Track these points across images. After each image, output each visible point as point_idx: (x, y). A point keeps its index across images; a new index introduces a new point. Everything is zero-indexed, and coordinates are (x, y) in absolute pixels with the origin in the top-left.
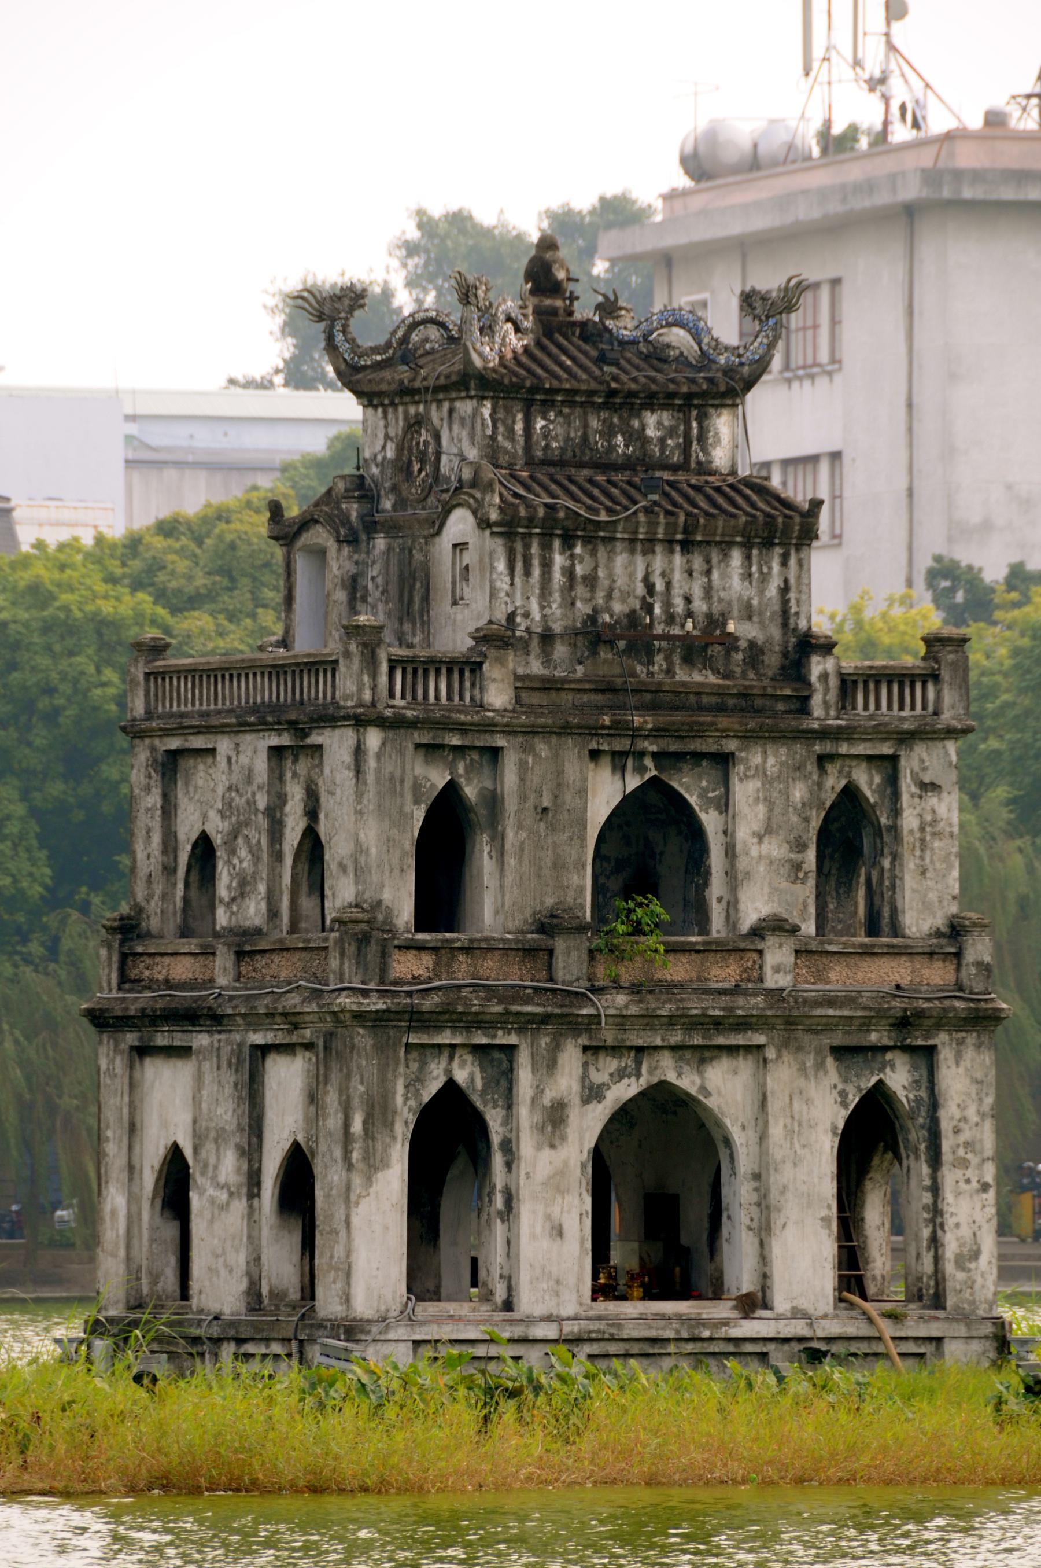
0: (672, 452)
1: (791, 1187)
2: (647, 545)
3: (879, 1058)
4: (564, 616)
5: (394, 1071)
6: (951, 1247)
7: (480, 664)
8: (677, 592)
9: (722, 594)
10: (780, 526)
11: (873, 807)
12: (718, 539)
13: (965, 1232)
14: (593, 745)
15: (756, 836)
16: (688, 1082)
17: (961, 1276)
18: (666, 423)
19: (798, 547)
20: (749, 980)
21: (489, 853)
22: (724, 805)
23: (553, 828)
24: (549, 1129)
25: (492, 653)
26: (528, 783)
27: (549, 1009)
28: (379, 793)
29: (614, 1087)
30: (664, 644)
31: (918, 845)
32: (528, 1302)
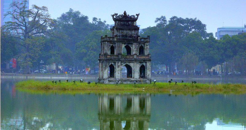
6: (147, 75)
15: (134, 49)
16: (129, 64)
22: (132, 46)
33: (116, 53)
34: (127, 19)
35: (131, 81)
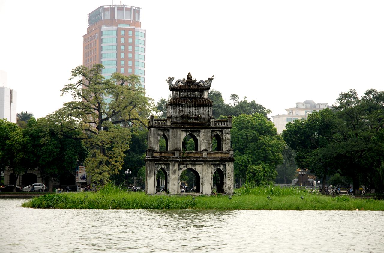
8: (194, 112)
14: (182, 129)
16: (193, 168)
17: (228, 190)
19: (210, 107)
22: (200, 136)
30: (192, 118)
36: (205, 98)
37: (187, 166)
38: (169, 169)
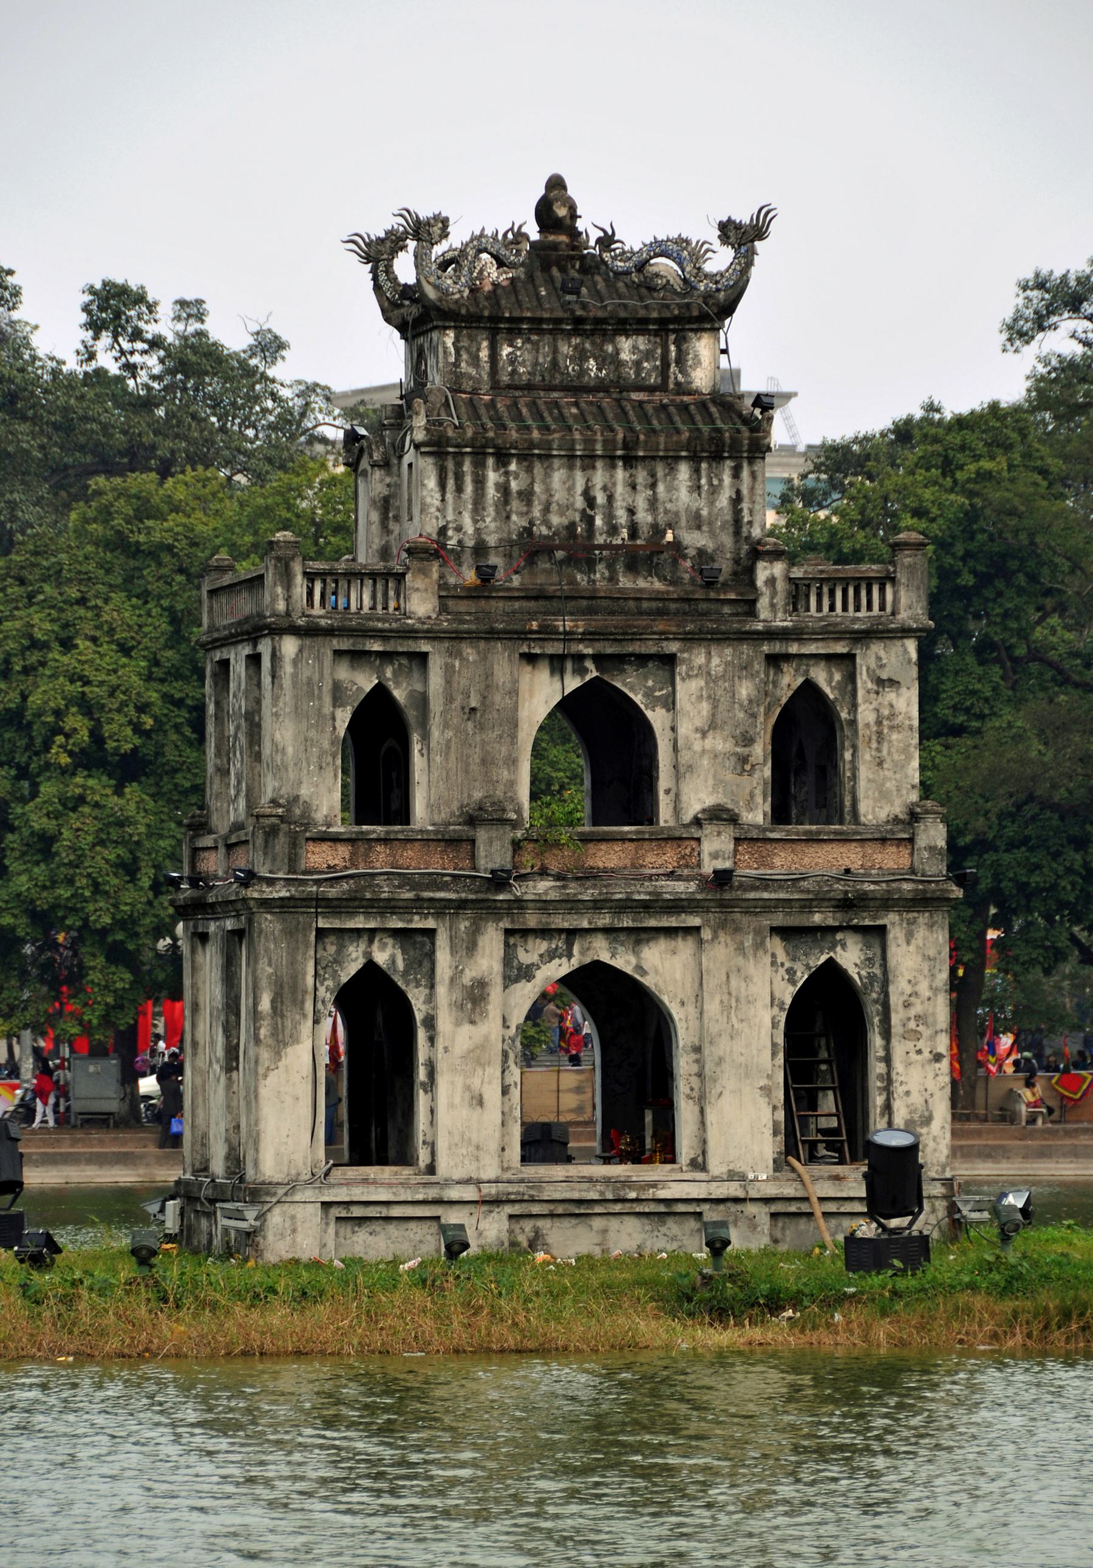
0: (649, 374)
1: (728, 1059)
2: (587, 461)
3: (829, 938)
4: (498, 529)
5: (305, 953)
7: (403, 575)
9: (669, 506)
10: (728, 441)
11: (833, 702)
12: (661, 454)
13: (916, 1099)
14: (525, 649)
15: (704, 737)
16: (623, 961)
18: (642, 347)
19: (751, 460)
20: (687, 866)
21: (420, 751)
22: (670, 703)
23: (481, 727)
24: (469, 1006)
25: (416, 564)
26: (455, 685)
27: (463, 895)
28: (296, 696)
29: (543, 967)
31: (874, 737)
32: (445, 1167)
33: (428, 800)
34: (589, 301)
35: (667, 1211)
36: (696, 392)
37: (576, 950)
38: (433, 970)
